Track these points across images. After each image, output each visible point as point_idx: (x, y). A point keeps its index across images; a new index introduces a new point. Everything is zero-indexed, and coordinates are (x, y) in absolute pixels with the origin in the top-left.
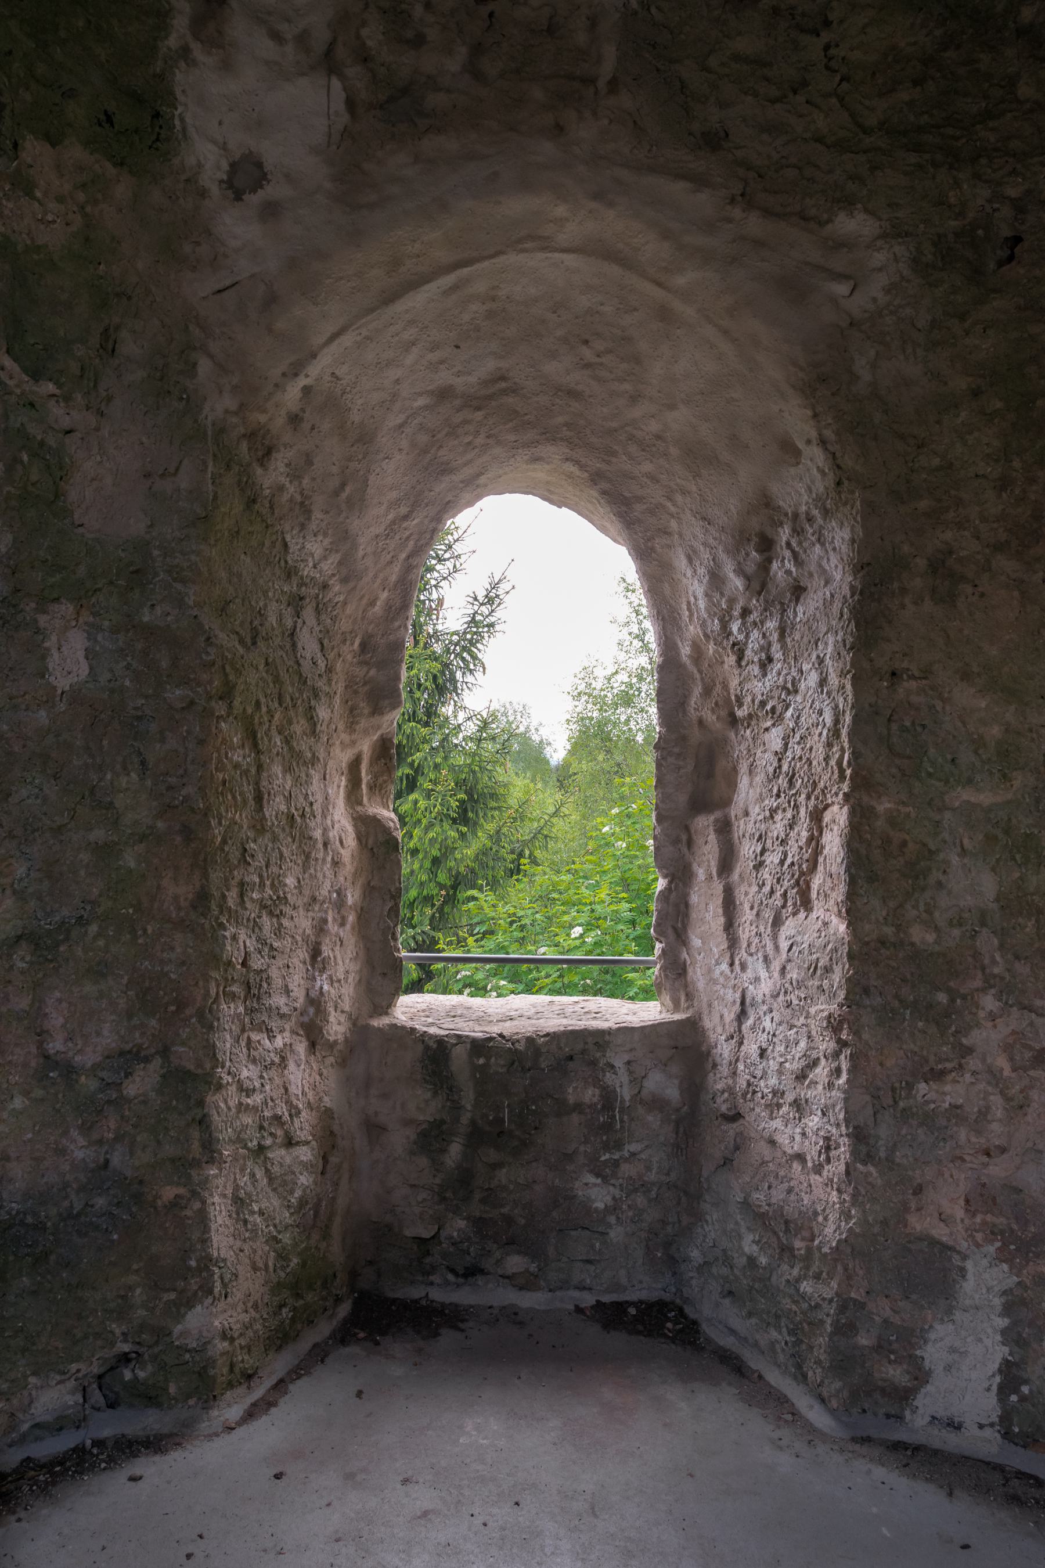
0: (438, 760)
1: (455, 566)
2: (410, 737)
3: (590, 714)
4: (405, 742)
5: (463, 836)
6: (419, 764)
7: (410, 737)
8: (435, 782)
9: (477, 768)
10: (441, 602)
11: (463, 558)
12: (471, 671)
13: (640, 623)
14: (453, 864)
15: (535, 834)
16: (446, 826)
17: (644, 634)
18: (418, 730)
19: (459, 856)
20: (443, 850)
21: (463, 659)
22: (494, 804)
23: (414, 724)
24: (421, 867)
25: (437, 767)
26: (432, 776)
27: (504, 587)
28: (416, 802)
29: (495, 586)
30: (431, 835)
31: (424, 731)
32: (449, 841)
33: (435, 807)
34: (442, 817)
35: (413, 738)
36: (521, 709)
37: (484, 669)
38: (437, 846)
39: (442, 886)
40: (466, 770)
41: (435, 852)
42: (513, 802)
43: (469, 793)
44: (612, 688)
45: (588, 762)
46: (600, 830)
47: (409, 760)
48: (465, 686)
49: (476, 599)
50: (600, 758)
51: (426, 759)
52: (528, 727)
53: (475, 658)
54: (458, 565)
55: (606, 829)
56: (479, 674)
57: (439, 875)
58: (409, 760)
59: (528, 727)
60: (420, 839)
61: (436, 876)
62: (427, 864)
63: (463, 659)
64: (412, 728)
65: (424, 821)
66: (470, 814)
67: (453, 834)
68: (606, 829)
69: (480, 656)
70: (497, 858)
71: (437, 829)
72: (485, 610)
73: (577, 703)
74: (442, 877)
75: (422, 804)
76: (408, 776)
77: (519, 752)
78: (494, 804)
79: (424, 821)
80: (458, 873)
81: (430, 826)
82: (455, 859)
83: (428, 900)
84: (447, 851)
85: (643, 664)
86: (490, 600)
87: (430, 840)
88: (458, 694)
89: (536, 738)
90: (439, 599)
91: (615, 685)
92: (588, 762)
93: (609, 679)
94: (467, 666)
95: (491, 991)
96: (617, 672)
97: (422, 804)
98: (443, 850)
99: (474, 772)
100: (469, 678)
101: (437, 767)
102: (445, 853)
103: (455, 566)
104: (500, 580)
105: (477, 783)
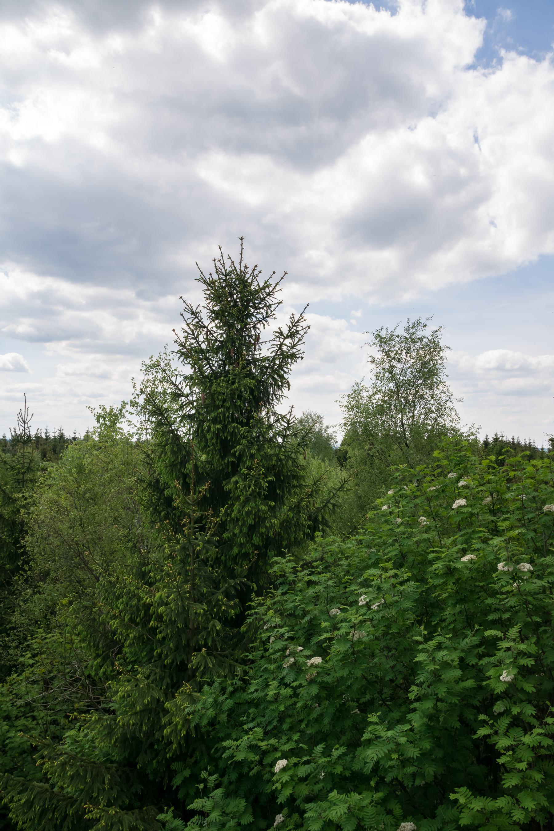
0: (253, 451)
1: (267, 313)
2: (233, 434)
3: (359, 420)
4: (229, 438)
5: (272, 509)
6: (239, 454)
7: (233, 434)
8: (249, 468)
9: (283, 457)
10: (257, 338)
11: (273, 307)
12: (279, 387)
13: (390, 362)
14: (263, 530)
15: (326, 503)
16: (259, 502)
17: (392, 369)
18: (238, 429)
19: (268, 525)
20: (257, 520)
21: (273, 379)
22: (296, 483)
23: (235, 424)
24: (241, 531)
25: (252, 456)
26: (248, 463)
27: (303, 324)
28: (237, 482)
29: (295, 324)
30: (247, 509)
31: (242, 429)
32: (261, 514)
33: (249, 487)
34: (255, 495)
35: (236, 435)
36: (316, 419)
37: (289, 386)
38: (252, 517)
39: (256, 547)
40: (275, 458)
41: (250, 521)
42: (309, 481)
43: (277, 475)
44: (373, 403)
45: (359, 450)
46: (380, 509)
47: (232, 451)
48: (274, 398)
49: (281, 334)
50: (367, 447)
51: (244, 450)
52: (320, 429)
53: (282, 377)
54: (269, 312)
55: (385, 508)
56: (285, 390)
57: (254, 538)
58: (232, 451)
59: (320, 429)
60: (239, 511)
61: (252, 539)
62: (245, 530)
63: (273, 379)
64: (234, 428)
65: (242, 498)
66: (278, 491)
67: (263, 507)
68: (385, 508)
69: (286, 376)
70: (298, 525)
71: (252, 504)
72: (288, 341)
73: (351, 413)
74: (256, 540)
75: (241, 484)
76: (233, 462)
77: (315, 443)
78: (296, 483)
79: (242, 498)
80: (268, 537)
81: (247, 501)
82: (266, 527)
83: (246, 555)
84: (260, 520)
85: (392, 388)
86: (291, 335)
87: (246, 512)
88: (269, 403)
89: (325, 435)
90: (256, 335)
91: (375, 401)
92: (359, 450)
93: (370, 398)
94: (276, 384)
95: (289, 655)
96: (376, 393)
97: (241, 484)
98: (257, 520)
99: (281, 460)
100: (278, 392)
101: (252, 456)
102: (258, 522)
103: (267, 313)
104: (299, 320)
105: (283, 468)
